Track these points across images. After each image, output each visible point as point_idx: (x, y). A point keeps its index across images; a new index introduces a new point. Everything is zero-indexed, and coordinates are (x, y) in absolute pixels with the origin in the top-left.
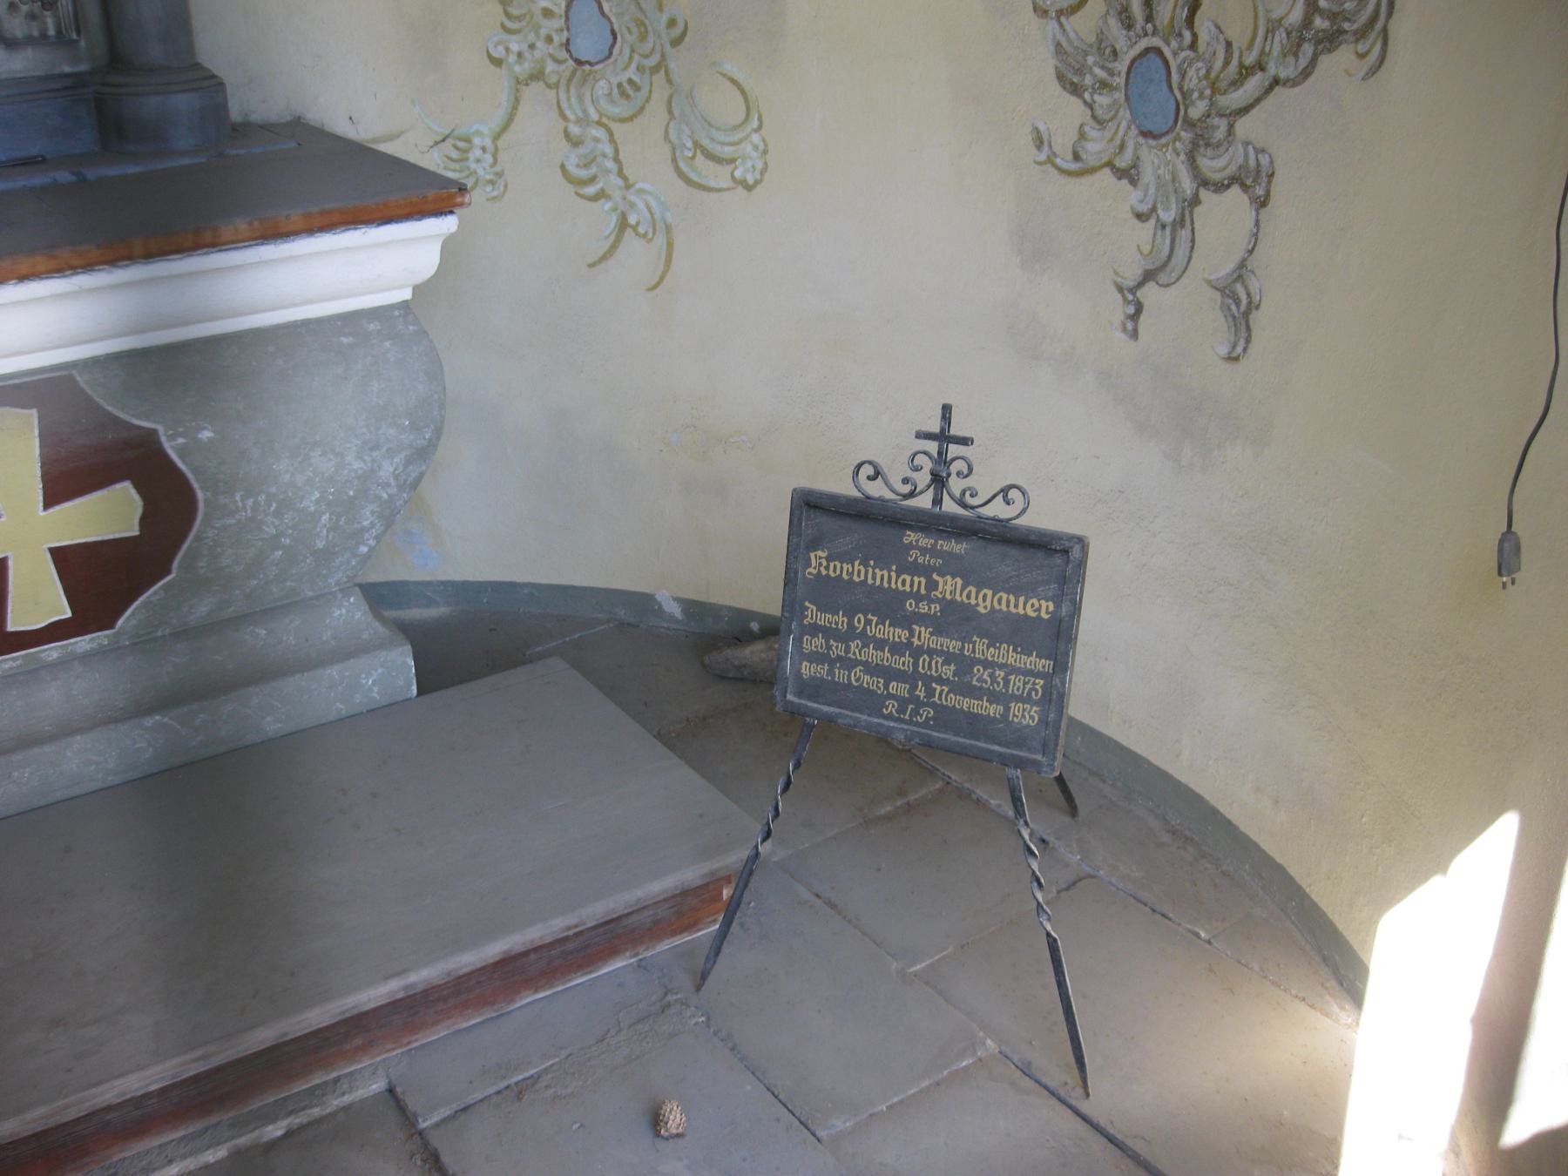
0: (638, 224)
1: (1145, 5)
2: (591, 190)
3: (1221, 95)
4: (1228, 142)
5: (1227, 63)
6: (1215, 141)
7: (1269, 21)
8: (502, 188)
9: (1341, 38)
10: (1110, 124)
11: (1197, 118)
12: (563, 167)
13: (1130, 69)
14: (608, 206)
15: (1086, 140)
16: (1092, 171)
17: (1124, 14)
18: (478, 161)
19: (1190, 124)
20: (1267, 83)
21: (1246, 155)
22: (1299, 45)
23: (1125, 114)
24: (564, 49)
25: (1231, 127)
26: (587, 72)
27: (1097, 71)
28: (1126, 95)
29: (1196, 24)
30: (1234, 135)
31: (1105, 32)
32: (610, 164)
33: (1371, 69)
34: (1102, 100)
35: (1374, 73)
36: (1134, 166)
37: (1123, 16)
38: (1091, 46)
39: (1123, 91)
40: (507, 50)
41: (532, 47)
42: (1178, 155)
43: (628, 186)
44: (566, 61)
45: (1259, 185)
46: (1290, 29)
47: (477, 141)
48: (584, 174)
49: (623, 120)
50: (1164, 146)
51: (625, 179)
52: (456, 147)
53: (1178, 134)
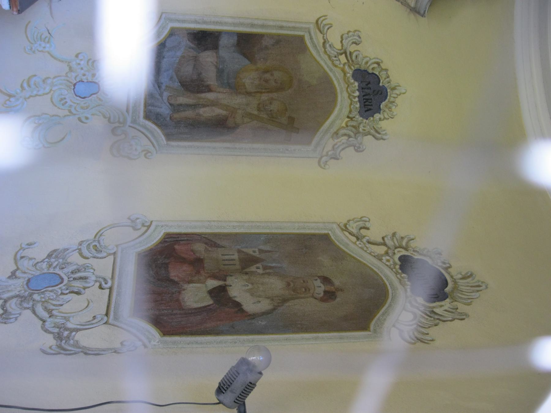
0: (10, 101)
1: (80, 277)
2: (25, 85)
3: (42, 304)
4: (22, 308)
5: (54, 305)
6: (23, 304)
7: (69, 317)
8: (29, 52)
9: (59, 340)
10: (35, 268)
11: (33, 297)
12: (35, 76)
13: (56, 274)
14: (18, 91)
15: (29, 260)
16: (16, 263)
17: (77, 271)
18: (40, 45)
19: (31, 295)
20: (44, 319)
21: (15, 314)
22: (58, 327)
23: (38, 273)
24: (80, 80)
25: (28, 308)
26: (71, 87)
27: (56, 263)
28: (45, 273)
29: (71, 294)
30: (24, 310)
31: (71, 265)
32: (35, 93)
33: (44, 351)
34: (44, 265)
35: (43, 352)
36: (16, 277)
37: (76, 271)
38: (66, 260)
39: (47, 272)
40: (81, 60)
41: (82, 69)
42: (19, 292)
43: (25, 99)
44: (76, 80)
45: (2, 319)
46: (65, 324)
47: (48, 45)
48: (32, 83)
49: (51, 99)
50: (23, 287)
51: (29, 98)
52: (46, 38)
53: (27, 291)
